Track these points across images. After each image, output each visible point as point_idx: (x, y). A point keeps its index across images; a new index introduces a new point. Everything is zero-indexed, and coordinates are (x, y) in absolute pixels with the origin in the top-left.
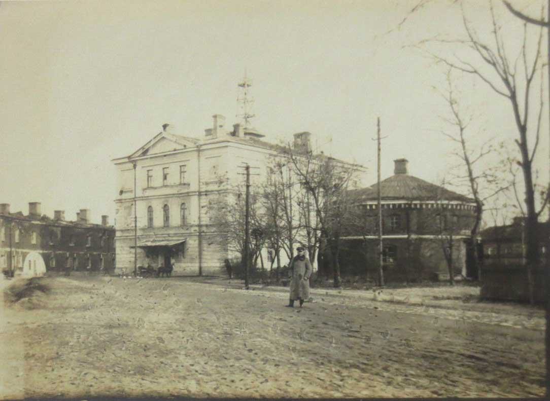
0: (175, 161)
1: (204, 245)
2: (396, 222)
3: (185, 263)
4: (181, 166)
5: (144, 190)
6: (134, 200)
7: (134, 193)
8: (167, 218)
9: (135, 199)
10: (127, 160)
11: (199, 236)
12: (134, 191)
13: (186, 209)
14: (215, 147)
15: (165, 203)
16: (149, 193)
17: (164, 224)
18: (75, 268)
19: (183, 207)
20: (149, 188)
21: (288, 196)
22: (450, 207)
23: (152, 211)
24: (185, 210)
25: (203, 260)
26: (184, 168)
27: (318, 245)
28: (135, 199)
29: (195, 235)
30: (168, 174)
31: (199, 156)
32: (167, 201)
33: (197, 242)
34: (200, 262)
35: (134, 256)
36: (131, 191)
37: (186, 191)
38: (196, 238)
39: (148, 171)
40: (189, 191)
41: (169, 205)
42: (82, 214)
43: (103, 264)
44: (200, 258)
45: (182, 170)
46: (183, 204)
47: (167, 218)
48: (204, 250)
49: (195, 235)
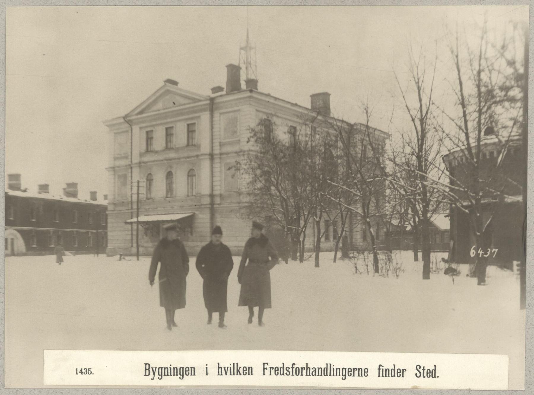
1: (218, 219)
3: (193, 241)
4: (188, 125)
7: (130, 160)
8: (170, 189)
11: (214, 204)
12: (130, 157)
13: (195, 175)
15: (169, 170)
16: (147, 158)
19: (191, 174)
23: (152, 180)
24: (194, 178)
27: (499, 193)
29: (206, 208)
31: (247, 41)
32: (171, 167)
35: (130, 233)
37: (195, 153)
38: (208, 211)
40: (199, 153)
42: (71, 189)
43: (91, 241)
45: (190, 130)
46: (192, 170)
47: (170, 189)
48: (511, 103)
49: (206, 208)
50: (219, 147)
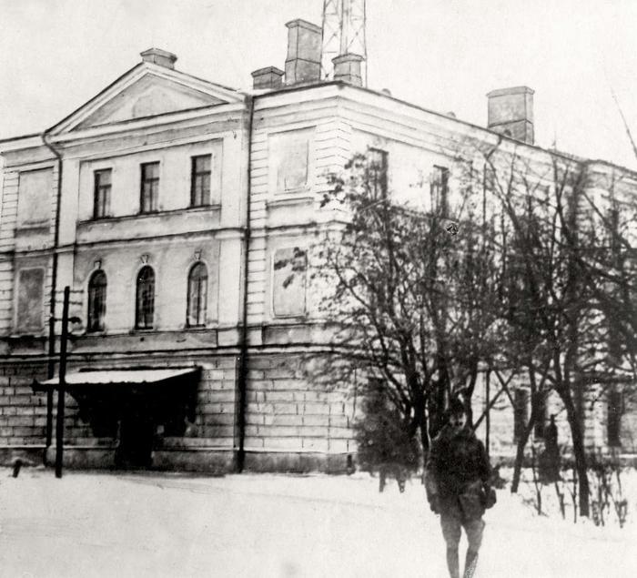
0: (179, 143)
2: (408, 452)
5: (81, 225)
6: (54, 252)
8: (145, 307)
9: (58, 251)
10: (38, 141)
12: (53, 230)
14: (186, 118)
17: (137, 321)
18: (597, 252)
20: (97, 218)
21: (589, 207)
22: (435, 456)
25: (251, 430)
26: (203, 164)
28: (58, 251)
30: (368, 146)
33: (232, 375)
34: (241, 436)
36: (43, 230)
39: (144, 166)
41: (156, 270)
44: (242, 423)
47: (145, 307)
50: (263, 213)
